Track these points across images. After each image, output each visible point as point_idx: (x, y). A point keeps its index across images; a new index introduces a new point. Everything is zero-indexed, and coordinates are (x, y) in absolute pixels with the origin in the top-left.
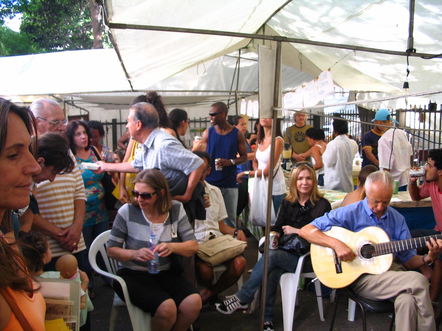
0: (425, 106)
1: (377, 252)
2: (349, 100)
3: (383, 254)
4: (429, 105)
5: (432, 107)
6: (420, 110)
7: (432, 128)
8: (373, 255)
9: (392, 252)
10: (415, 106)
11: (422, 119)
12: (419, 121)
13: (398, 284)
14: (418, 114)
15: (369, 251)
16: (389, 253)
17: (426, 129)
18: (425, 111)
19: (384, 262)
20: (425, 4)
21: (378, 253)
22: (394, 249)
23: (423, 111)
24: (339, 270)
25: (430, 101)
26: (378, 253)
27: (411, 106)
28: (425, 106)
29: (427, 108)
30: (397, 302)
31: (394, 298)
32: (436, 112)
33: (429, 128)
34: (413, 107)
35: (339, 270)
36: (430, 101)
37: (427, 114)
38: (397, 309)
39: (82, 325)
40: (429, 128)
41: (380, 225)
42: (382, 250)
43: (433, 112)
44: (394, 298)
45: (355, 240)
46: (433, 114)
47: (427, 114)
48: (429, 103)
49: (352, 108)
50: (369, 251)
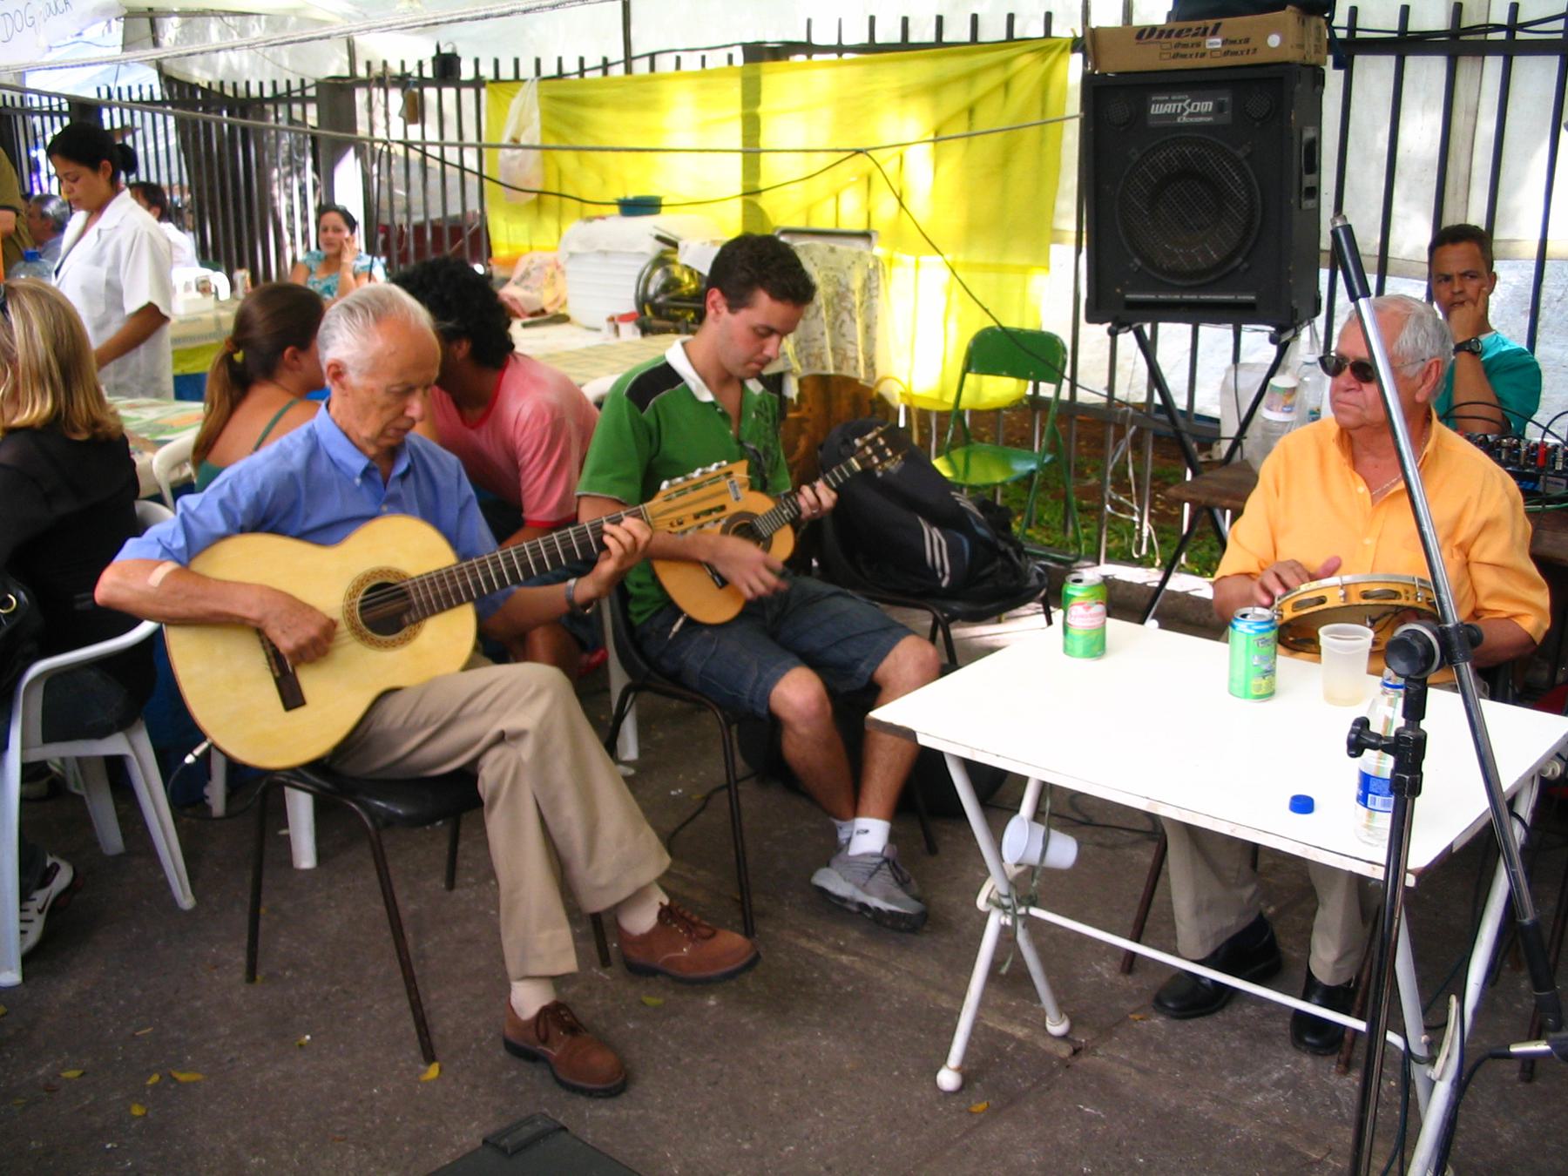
0: (420, 64)
1: (421, 603)
2: (126, 45)
3: (442, 610)
4: (434, 59)
5: (446, 67)
6: (403, 81)
7: (451, 135)
8: (406, 618)
9: (470, 599)
10: (385, 63)
11: (414, 112)
12: (401, 121)
13: (486, 710)
14: (396, 97)
15: (388, 609)
16: (460, 602)
17: (428, 139)
18: (423, 82)
19: (450, 635)
20: (1065, 351)
21: (423, 610)
22: (477, 584)
23: (415, 84)
24: (292, 697)
25: (438, 48)
26: (423, 610)
27: (369, 64)
28: (420, 64)
29: (428, 72)
30: (488, 776)
31: (475, 761)
32: (460, 85)
33: (442, 135)
34: (377, 69)
35: (292, 697)
36: (438, 48)
37: (430, 93)
38: (493, 799)
39: (25, 948)
40: (442, 135)
41: (396, 504)
42: (439, 595)
43: (448, 85)
44: (475, 761)
45: (321, 577)
46: (449, 93)
47: (430, 93)
48: (434, 53)
49: (146, 81)
50: (388, 609)
